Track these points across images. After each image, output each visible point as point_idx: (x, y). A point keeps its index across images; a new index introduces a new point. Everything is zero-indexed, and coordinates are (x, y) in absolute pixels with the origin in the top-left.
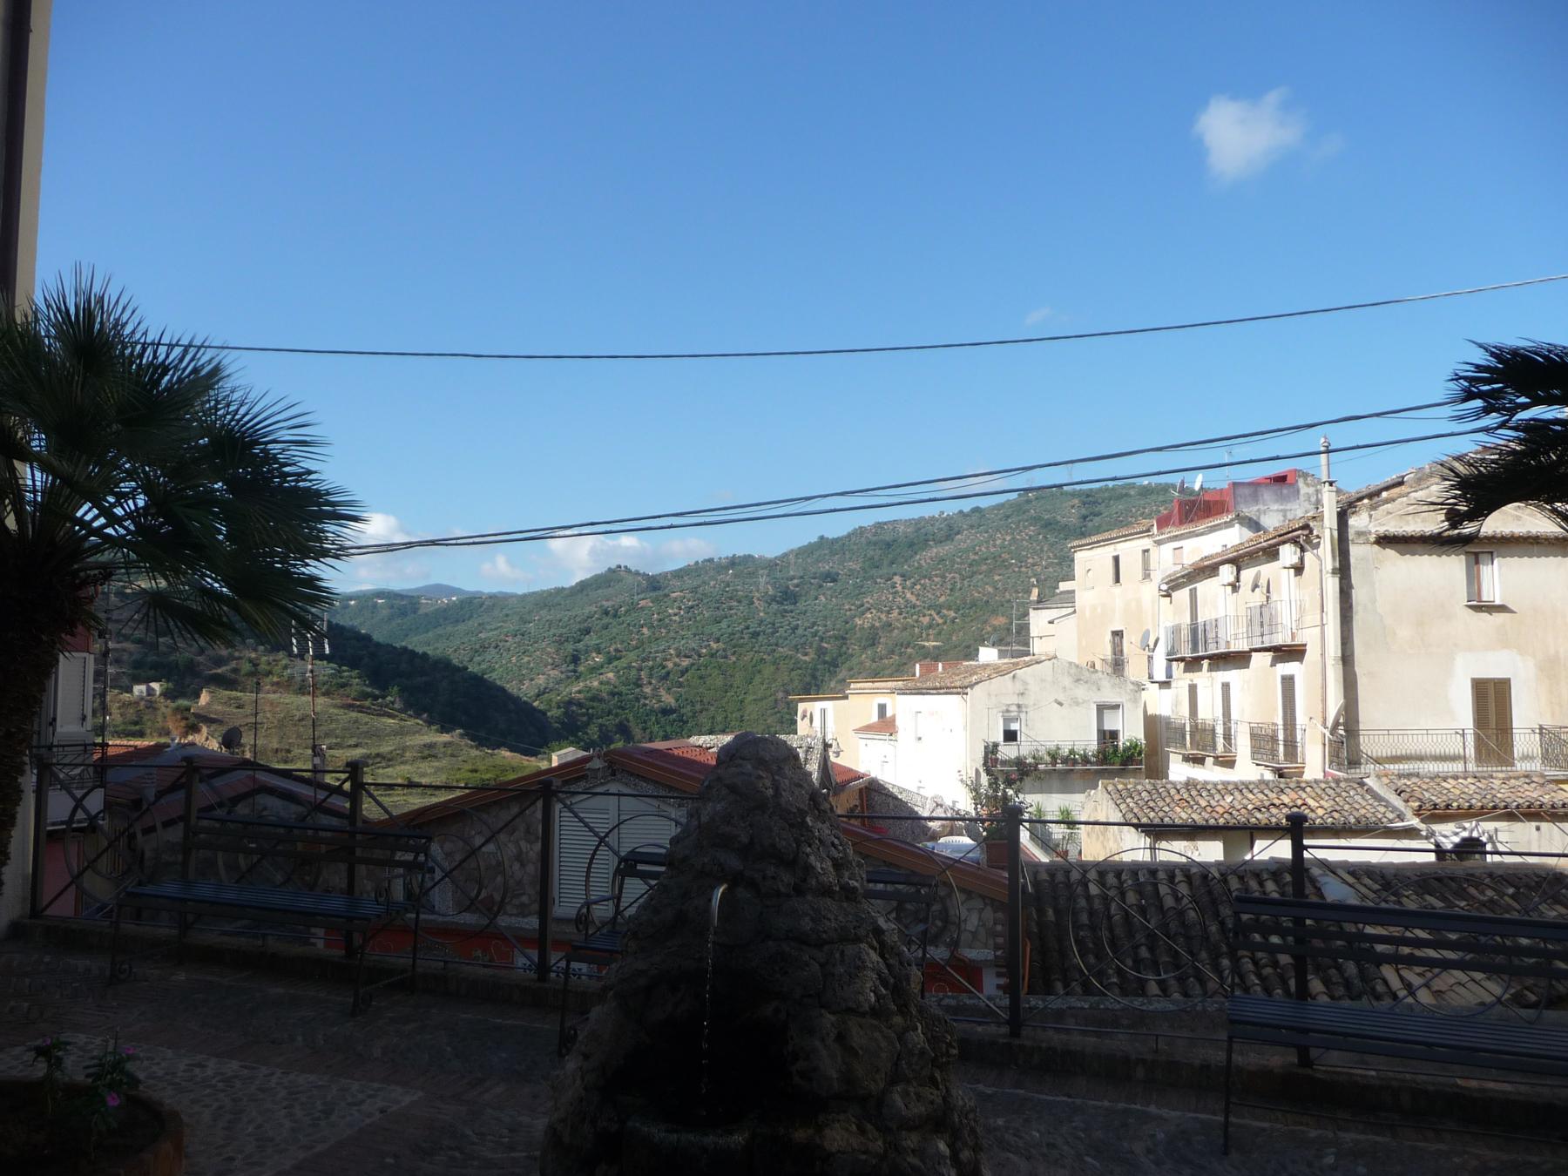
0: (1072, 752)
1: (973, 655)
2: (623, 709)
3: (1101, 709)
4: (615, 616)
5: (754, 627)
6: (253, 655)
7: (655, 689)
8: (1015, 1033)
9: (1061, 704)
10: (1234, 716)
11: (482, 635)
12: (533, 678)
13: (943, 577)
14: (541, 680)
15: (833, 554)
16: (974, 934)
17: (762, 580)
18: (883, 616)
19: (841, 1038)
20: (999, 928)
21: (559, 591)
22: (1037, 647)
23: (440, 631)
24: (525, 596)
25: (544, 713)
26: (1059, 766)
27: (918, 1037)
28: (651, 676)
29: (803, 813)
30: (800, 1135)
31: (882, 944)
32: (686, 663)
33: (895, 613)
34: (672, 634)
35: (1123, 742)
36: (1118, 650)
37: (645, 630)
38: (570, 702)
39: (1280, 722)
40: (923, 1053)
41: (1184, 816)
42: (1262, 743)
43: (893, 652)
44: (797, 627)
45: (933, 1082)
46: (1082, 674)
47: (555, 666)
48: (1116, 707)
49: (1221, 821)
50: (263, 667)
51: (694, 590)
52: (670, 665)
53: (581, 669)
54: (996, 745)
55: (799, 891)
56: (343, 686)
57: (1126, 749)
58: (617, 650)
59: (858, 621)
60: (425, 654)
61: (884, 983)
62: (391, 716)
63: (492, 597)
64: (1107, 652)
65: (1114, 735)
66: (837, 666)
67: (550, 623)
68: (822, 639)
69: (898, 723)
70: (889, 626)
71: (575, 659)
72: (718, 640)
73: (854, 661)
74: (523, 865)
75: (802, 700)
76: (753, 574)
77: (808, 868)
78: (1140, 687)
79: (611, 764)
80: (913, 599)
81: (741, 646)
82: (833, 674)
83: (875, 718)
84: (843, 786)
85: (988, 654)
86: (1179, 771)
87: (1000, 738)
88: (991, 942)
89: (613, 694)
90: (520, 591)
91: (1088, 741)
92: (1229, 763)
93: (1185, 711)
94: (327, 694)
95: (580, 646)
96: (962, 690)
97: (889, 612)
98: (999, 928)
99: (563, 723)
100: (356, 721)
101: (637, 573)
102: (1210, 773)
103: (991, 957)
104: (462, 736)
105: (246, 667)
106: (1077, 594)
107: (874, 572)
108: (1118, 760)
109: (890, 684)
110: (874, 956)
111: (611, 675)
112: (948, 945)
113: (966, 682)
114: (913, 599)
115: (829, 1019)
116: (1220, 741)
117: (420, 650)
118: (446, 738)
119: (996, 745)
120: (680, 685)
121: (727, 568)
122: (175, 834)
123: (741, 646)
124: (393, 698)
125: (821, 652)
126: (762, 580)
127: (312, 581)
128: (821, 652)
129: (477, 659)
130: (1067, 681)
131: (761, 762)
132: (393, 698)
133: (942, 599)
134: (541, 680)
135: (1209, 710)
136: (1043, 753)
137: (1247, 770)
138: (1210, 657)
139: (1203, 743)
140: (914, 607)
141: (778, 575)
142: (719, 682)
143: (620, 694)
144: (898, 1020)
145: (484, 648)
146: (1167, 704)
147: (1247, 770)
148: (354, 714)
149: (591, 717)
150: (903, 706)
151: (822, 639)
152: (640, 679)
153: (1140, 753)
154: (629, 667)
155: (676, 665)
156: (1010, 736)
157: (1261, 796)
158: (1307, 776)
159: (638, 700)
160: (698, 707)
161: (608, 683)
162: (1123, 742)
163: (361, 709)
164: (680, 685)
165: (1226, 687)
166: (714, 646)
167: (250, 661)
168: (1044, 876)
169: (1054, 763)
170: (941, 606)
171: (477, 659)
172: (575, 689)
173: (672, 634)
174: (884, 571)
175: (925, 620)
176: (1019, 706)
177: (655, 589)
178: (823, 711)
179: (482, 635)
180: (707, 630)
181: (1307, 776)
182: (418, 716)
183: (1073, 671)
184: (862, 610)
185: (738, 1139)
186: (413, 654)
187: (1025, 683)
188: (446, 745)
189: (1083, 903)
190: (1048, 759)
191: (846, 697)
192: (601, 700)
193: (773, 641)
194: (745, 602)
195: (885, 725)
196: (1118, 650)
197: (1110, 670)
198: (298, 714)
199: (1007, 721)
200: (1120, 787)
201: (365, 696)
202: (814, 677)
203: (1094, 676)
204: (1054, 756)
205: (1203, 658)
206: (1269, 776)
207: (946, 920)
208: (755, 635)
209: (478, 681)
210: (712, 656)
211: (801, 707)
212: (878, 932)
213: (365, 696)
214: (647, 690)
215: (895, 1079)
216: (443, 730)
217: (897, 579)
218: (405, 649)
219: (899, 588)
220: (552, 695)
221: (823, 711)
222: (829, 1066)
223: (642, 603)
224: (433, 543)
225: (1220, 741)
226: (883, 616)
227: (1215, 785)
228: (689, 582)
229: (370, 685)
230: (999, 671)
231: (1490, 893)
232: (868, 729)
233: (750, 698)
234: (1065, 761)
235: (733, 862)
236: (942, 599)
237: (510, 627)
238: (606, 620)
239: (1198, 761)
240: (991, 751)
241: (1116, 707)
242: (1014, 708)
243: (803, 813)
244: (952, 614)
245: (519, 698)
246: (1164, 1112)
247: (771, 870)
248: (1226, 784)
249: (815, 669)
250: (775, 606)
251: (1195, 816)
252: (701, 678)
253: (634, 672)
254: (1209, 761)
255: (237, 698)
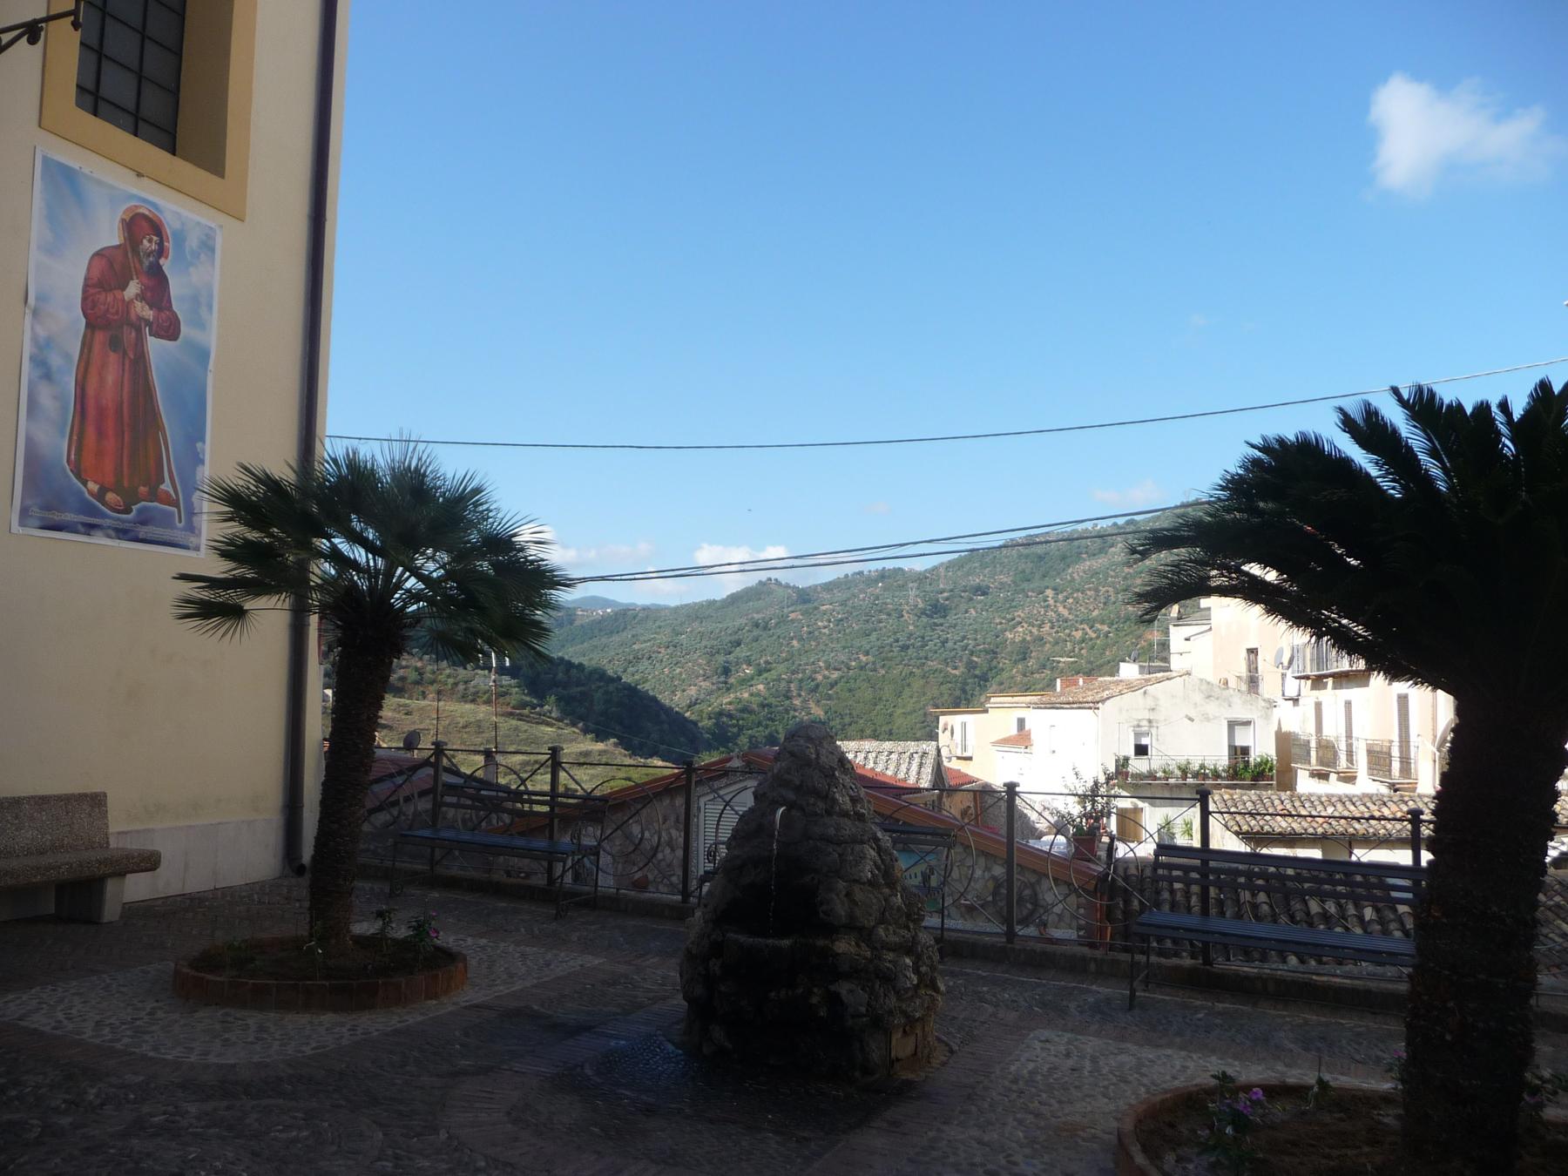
0: (1202, 766)
1: (1114, 671)
2: (773, 720)
3: (1232, 725)
4: (765, 628)
5: (902, 637)
6: (419, 664)
7: (805, 701)
8: (1010, 941)
9: (1191, 719)
10: (1413, 738)
11: (636, 647)
12: (685, 690)
13: (1097, 590)
14: (693, 691)
15: (984, 566)
16: (1060, 916)
17: (912, 593)
18: (1035, 630)
19: (847, 895)
20: (1082, 911)
21: (711, 603)
22: (1176, 663)
23: (595, 642)
24: (676, 609)
25: (695, 723)
26: (1190, 781)
27: (898, 900)
28: (800, 688)
29: (833, 769)
30: (821, 943)
31: (879, 847)
32: (835, 675)
33: (1047, 628)
34: (822, 647)
35: (1254, 758)
36: (1253, 668)
37: (795, 643)
38: (721, 714)
39: (1396, 738)
40: (899, 908)
41: (1284, 824)
42: (1379, 760)
43: (1044, 667)
44: (946, 641)
45: (908, 928)
46: (1216, 691)
47: (706, 678)
48: (1248, 723)
49: (1320, 830)
50: (428, 676)
51: (843, 603)
52: (819, 677)
53: (732, 680)
54: (1126, 759)
55: (829, 813)
56: (504, 694)
57: (1258, 765)
58: (767, 662)
59: (1009, 635)
60: (581, 665)
61: (878, 868)
62: (548, 724)
63: (645, 609)
64: (1243, 670)
65: (1245, 751)
66: (986, 680)
67: (702, 635)
68: (972, 653)
69: (1033, 736)
70: (1040, 639)
71: (726, 671)
72: (867, 653)
73: (1005, 675)
74: (673, 850)
75: (944, 714)
76: (903, 587)
77: (834, 801)
78: (1272, 704)
79: (748, 763)
80: (1066, 613)
81: (890, 659)
82: (983, 688)
83: (1014, 731)
84: (954, 790)
85: (1129, 671)
86: (1305, 784)
87: (1131, 752)
88: (1074, 924)
89: (763, 706)
90: (673, 603)
91: (1219, 758)
92: (1349, 779)
93: (1311, 728)
94: (488, 702)
95: (731, 657)
96: (1094, 705)
97: (1040, 626)
98: (1082, 911)
99: (713, 734)
100: (516, 729)
101: (787, 586)
102: (1334, 787)
103: (1074, 937)
104: (616, 745)
105: (413, 676)
106: (1213, 612)
107: (1025, 585)
108: (1248, 775)
109: (1028, 699)
110: (873, 853)
111: (761, 687)
112: (1037, 926)
113: (1097, 698)
114: (1066, 613)
115: (841, 885)
116: (1396, 765)
117: (576, 661)
118: (600, 746)
119: (1126, 759)
120: (830, 698)
121: (877, 581)
122: (424, 805)
123: (890, 659)
124: (551, 707)
125: (971, 666)
126: (912, 593)
127: (538, 624)
128: (971, 666)
129: (631, 669)
130: (1198, 697)
131: (809, 739)
132: (551, 707)
133: (1096, 613)
134: (693, 691)
135: (1333, 729)
136: (1173, 767)
137: (1366, 784)
138: (1333, 675)
139: (1327, 762)
140: (1066, 621)
141: (928, 588)
142: (868, 694)
143: (769, 706)
144: (886, 891)
145: (638, 659)
146: (1298, 721)
147: (1366, 784)
148: (514, 722)
149: (741, 729)
150: (1038, 720)
151: (972, 653)
152: (789, 690)
153: (1271, 769)
154: (779, 680)
155: (825, 677)
156: (1141, 750)
157: (1362, 808)
158: (1420, 790)
159: (787, 711)
160: (847, 720)
161: (758, 695)
162: (1254, 758)
163: (521, 718)
164: (830, 698)
165: (1348, 704)
166: (864, 659)
167: (417, 669)
168: (1133, 871)
169: (1185, 777)
170: (1095, 620)
171: (631, 669)
172: (726, 701)
173: (822, 647)
174: (1035, 584)
175: (1078, 635)
176: (1150, 721)
177: (805, 601)
178: (964, 725)
179: (636, 647)
180: (857, 643)
181: (1420, 790)
182: (574, 725)
183: (1204, 687)
184: (1014, 624)
185: (786, 943)
186: (569, 665)
187: (1155, 698)
188: (601, 753)
189: (1166, 895)
190: (1179, 773)
191: (986, 711)
192: (751, 712)
193: (922, 654)
194: (895, 615)
195: (1021, 738)
196: (1253, 668)
197: (1244, 687)
198: (462, 722)
199: (1138, 735)
200: (1226, 797)
201: (523, 705)
202: (964, 691)
203: (1226, 693)
204: (1184, 772)
205: (1326, 676)
206: (1384, 790)
207: (1036, 904)
208: (905, 648)
209: (632, 691)
210: (862, 668)
211: (942, 719)
212: (877, 840)
213: (523, 705)
214: (797, 702)
215: (882, 920)
216: (600, 736)
217: (1049, 592)
218: (562, 659)
219: (1051, 602)
220: (703, 706)
221: (964, 725)
222: (841, 909)
223: (792, 616)
224: (603, 578)
225: (1396, 765)
226: (1035, 630)
227: (1319, 797)
228: (839, 595)
229: (529, 694)
230: (1131, 687)
231: (1558, 899)
232: (1006, 741)
233: (899, 711)
234: (1196, 775)
235: (791, 796)
236: (1096, 613)
237: (663, 638)
238: (756, 632)
239: (1324, 776)
240: (1122, 763)
241: (1248, 723)
242: (1145, 723)
243: (833, 769)
244: (1106, 628)
245: (671, 709)
246: (1100, 989)
247: (812, 800)
248: (1329, 797)
249: (965, 683)
250: (924, 619)
251: (1295, 825)
252: (850, 690)
253: (783, 684)
254: (1333, 777)
255: (406, 705)
